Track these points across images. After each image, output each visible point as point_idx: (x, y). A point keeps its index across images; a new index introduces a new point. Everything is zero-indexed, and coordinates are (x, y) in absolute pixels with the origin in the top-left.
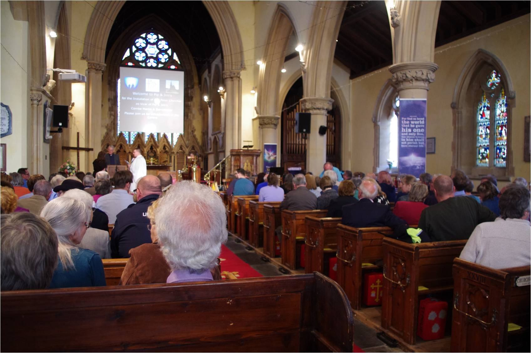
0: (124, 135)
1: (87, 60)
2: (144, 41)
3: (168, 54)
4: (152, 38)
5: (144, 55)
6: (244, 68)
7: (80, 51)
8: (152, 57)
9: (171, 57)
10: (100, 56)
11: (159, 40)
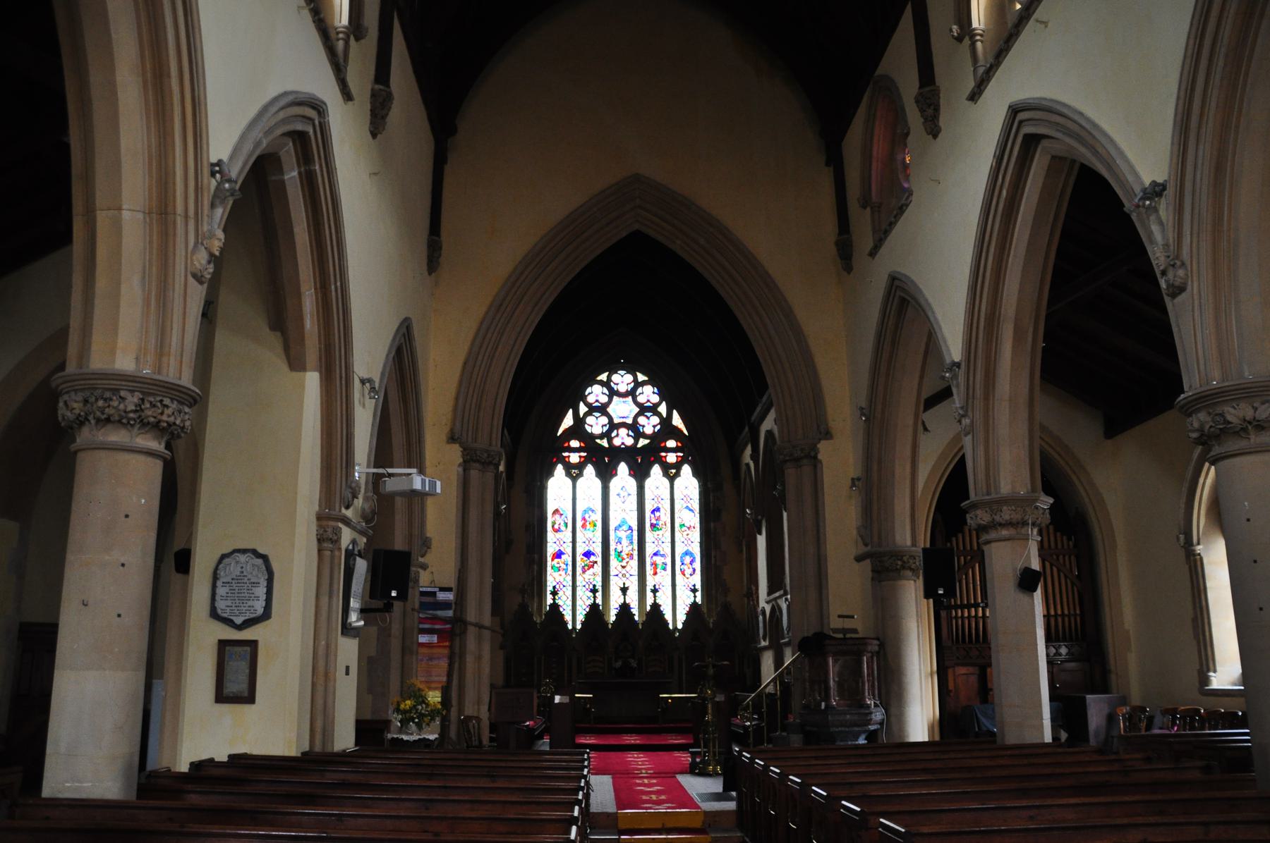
0: (561, 610)
1: (461, 445)
2: (605, 391)
3: (659, 415)
4: (622, 380)
5: (604, 420)
6: (828, 435)
7: (446, 424)
8: (623, 425)
9: (666, 422)
10: (491, 434)
11: (637, 384)
